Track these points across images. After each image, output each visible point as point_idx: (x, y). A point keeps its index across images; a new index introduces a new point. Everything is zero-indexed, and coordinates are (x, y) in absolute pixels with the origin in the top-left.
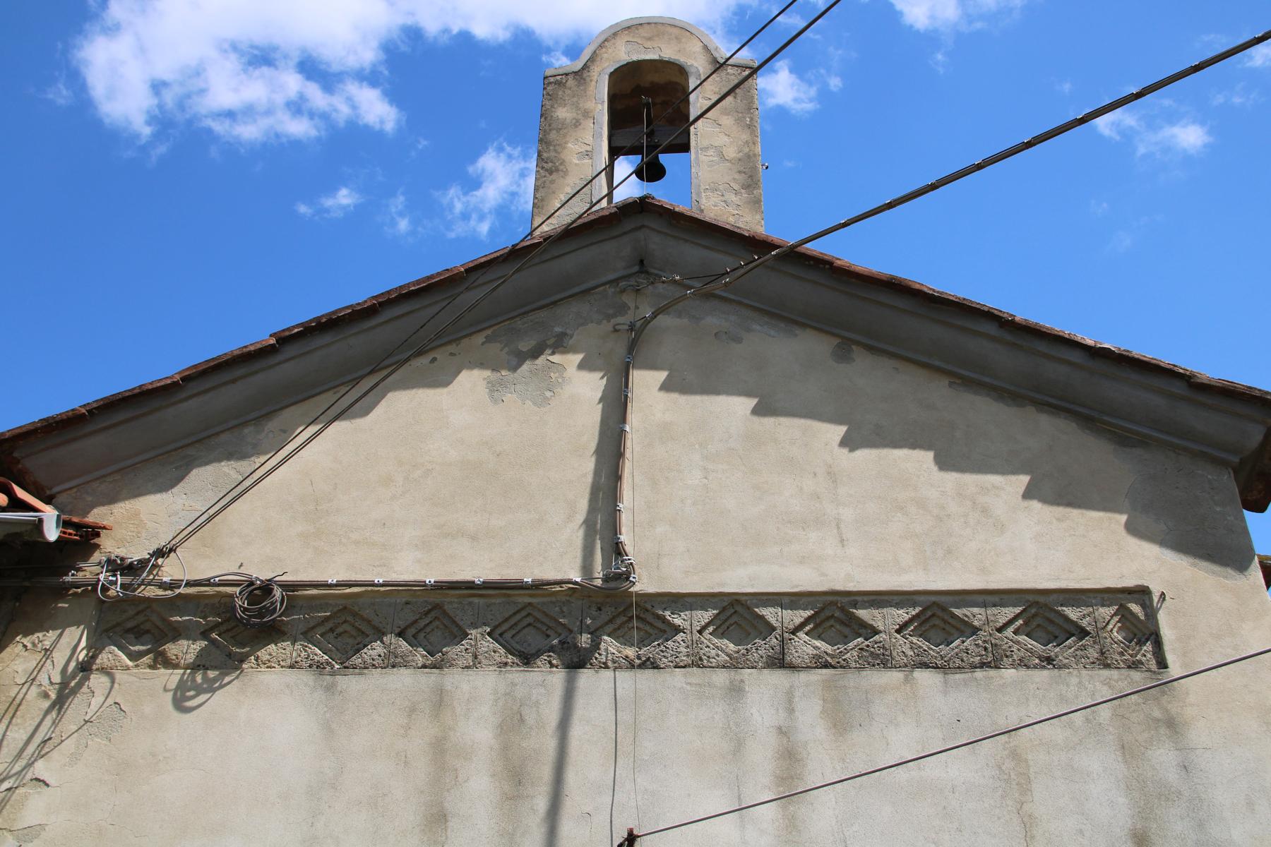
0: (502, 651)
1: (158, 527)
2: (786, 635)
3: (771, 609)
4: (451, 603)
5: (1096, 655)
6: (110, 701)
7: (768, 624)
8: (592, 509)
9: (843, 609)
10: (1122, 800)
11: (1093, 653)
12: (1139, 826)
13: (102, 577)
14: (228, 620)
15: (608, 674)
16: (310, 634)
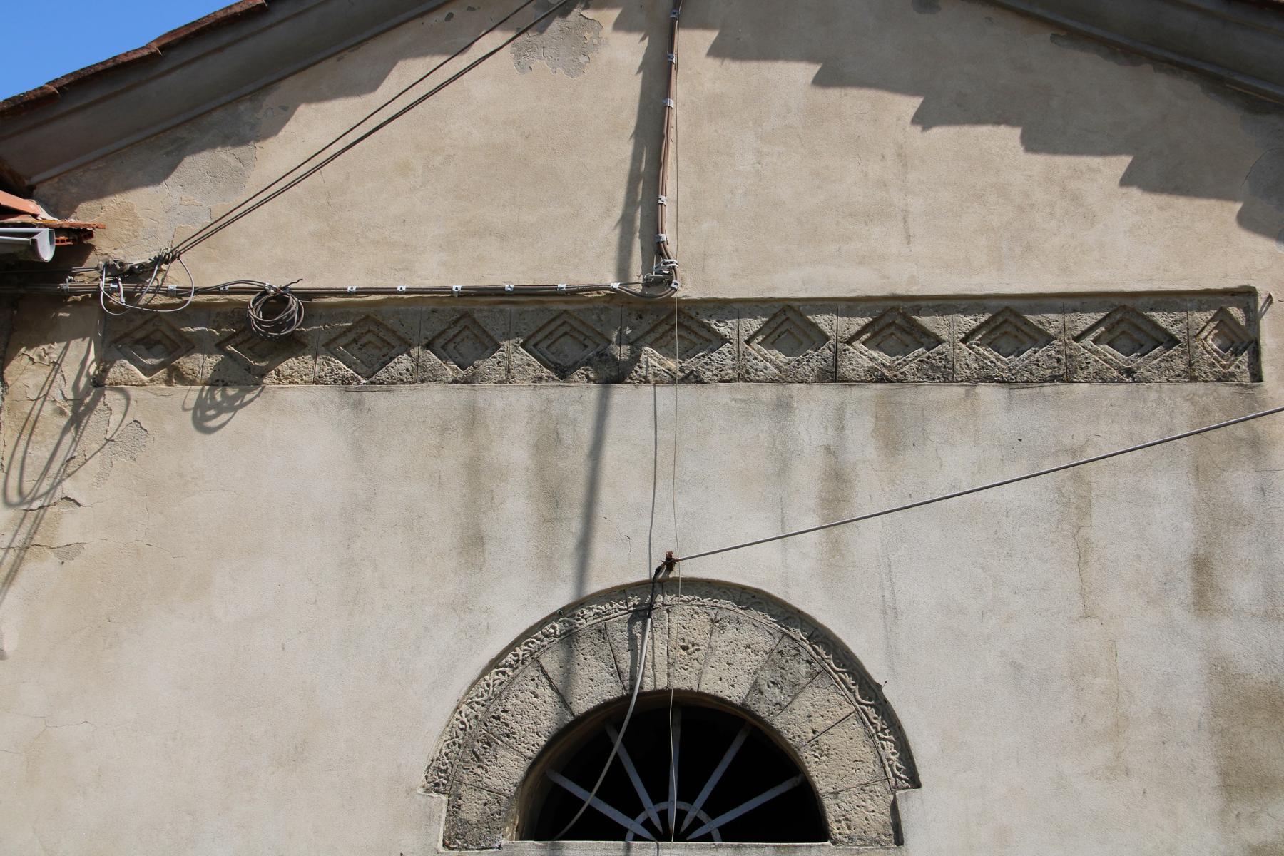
0: (537, 364)
1: (169, 222)
2: (840, 345)
3: (826, 317)
4: (481, 311)
5: (1183, 367)
6: (129, 419)
7: (822, 332)
8: (630, 202)
9: (904, 315)
10: (1187, 525)
11: (1180, 365)
12: (1202, 552)
13: (102, 285)
14: (244, 330)
15: (648, 389)
16: (332, 347)
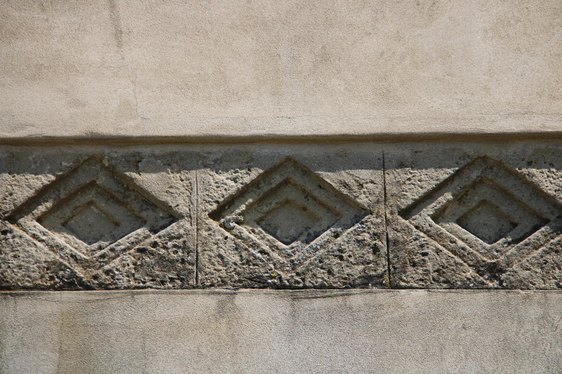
9: (112, 171)
